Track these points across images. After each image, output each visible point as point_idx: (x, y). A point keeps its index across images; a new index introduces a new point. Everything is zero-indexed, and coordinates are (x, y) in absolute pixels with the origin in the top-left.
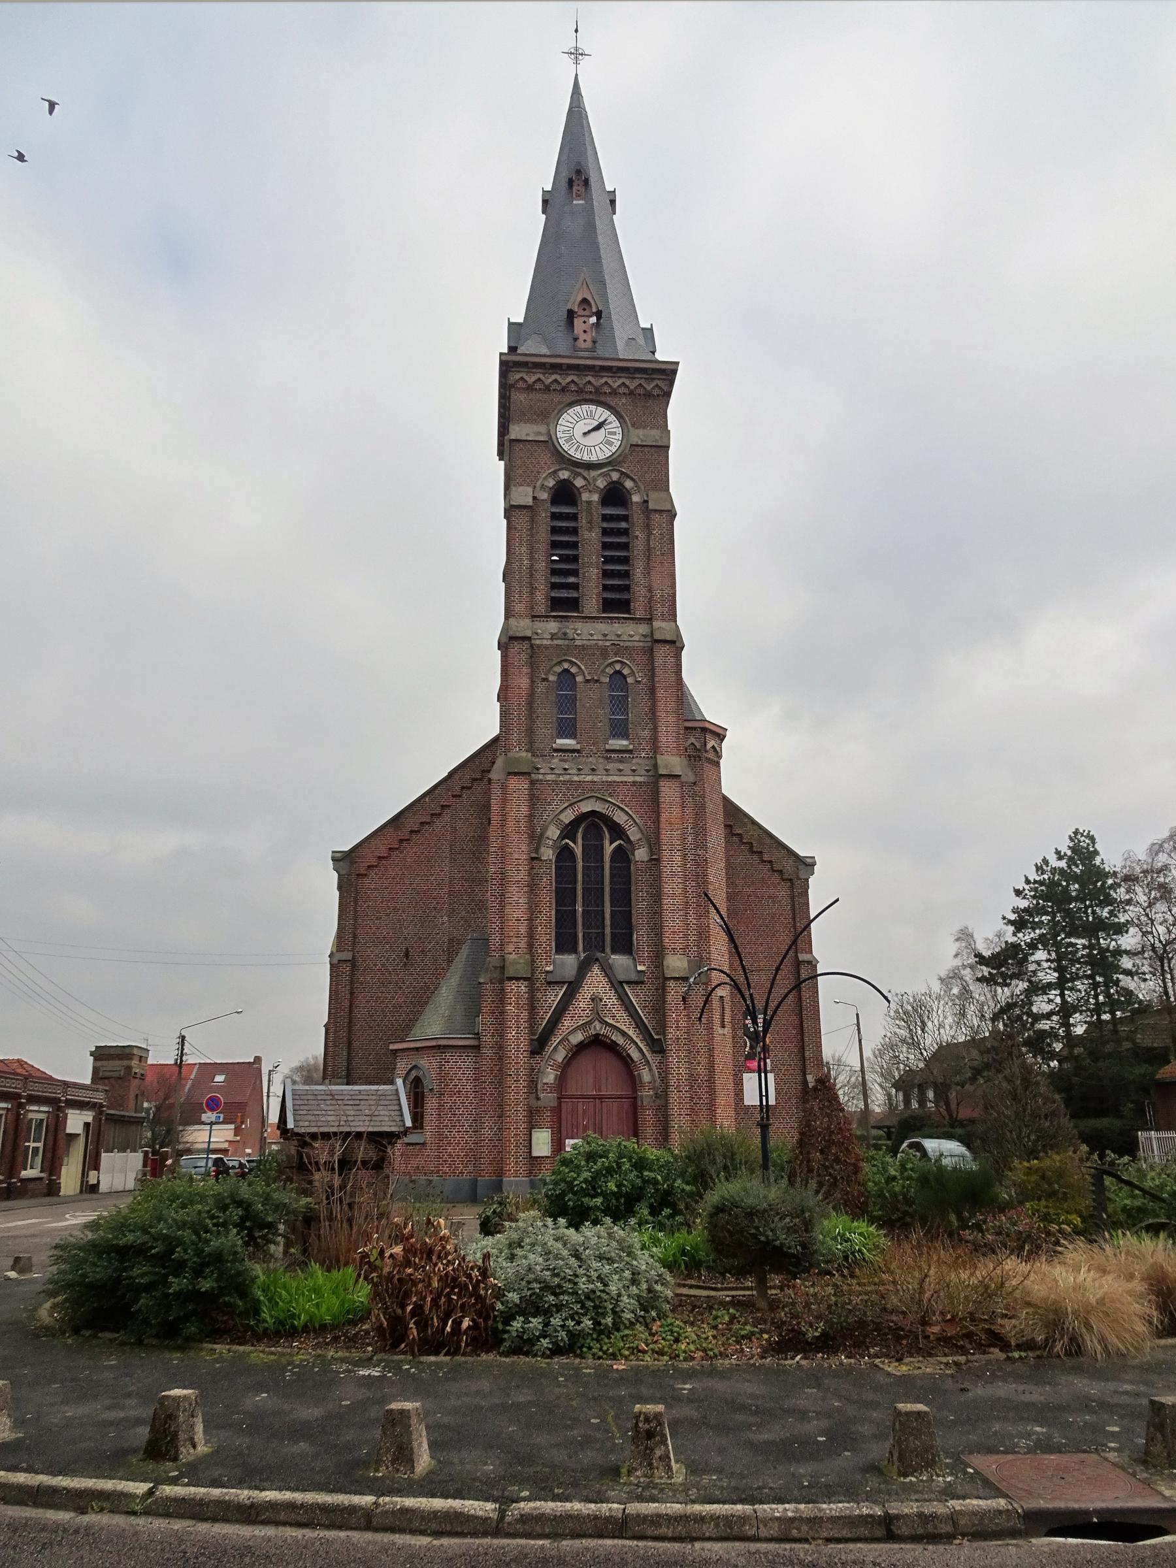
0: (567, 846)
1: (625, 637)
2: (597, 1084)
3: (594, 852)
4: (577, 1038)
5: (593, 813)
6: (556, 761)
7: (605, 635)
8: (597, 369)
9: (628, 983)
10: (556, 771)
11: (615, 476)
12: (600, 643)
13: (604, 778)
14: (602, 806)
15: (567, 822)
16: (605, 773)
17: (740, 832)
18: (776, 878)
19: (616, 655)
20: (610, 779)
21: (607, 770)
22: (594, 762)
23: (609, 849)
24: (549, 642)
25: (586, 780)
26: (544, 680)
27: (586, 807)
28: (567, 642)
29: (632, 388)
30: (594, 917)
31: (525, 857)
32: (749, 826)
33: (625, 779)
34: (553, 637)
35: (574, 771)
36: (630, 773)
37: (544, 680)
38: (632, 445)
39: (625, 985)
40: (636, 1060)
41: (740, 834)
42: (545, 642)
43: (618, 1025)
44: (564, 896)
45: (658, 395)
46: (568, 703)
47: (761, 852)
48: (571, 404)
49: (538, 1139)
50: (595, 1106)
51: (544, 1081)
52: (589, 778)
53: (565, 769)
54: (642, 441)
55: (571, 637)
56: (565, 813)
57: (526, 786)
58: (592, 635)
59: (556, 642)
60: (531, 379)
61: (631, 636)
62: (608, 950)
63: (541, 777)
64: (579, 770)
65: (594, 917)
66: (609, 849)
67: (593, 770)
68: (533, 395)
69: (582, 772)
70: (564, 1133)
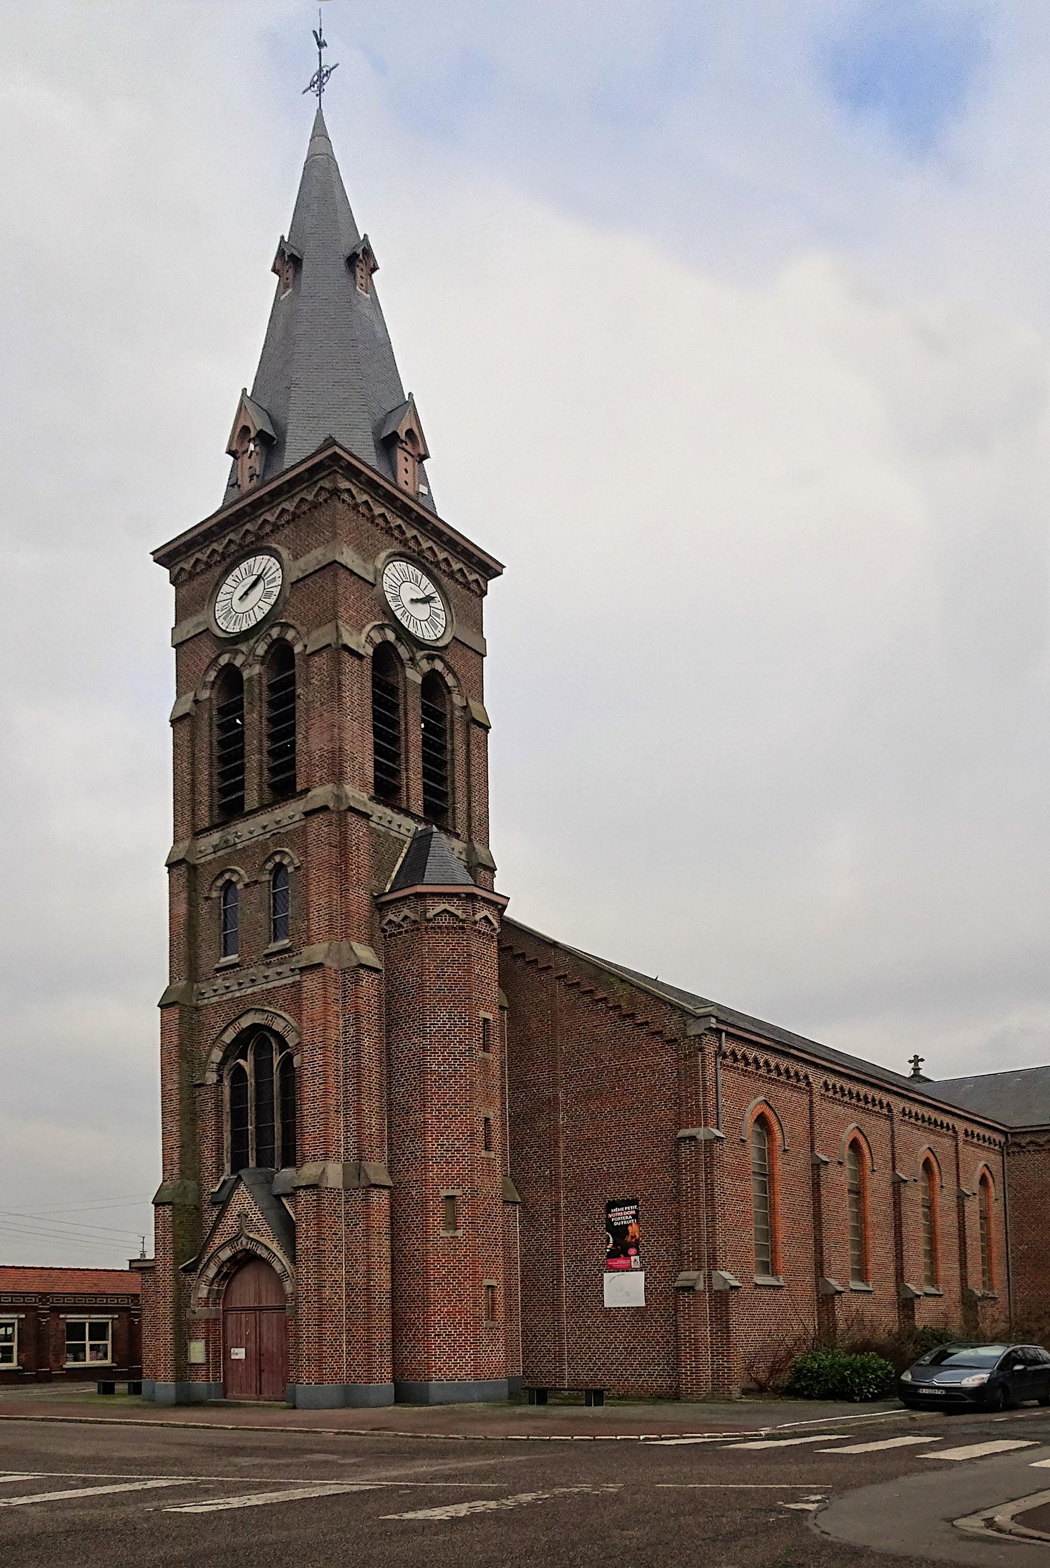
0: (239, 1065)
1: (285, 822)
2: (258, 1296)
3: (262, 1068)
4: (226, 1254)
5: (254, 1027)
6: (220, 981)
7: (264, 827)
8: (267, 499)
9: (286, 1195)
10: (220, 992)
11: (275, 632)
12: (261, 838)
13: (265, 987)
14: (262, 1017)
15: (228, 1042)
16: (264, 980)
17: (605, 995)
18: (657, 1043)
19: (276, 845)
20: (270, 986)
21: (266, 977)
22: (255, 972)
23: (277, 1059)
24: (213, 856)
25: (247, 993)
26: (207, 899)
27: (246, 1022)
28: (229, 850)
29: (292, 509)
30: (264, 1134)
31: (177, 1086)
32: (617, 985)
33: (285, 982)
34: (216, 849)
35: (236, 987)
36: (290, 973)
37: (207, 899)
38: (292, 584)
39: (284, 1201)
40: (279, 1272)
41: (605, 999)
42: (209, 858)
43: (261, 1239)
44: (238, 1118)
45: (325, 501)
46: (227, 920)
47: (633, 1015)
48: (227, 572)
49: (194, 1349)
50: (256, 1316)
51: (199, 1296)
52: (250, 991)
53: (228, 988)
54: (303, 571)
55: (232, 842)
56: (227, 1033)
57: (177, 1016)
58: (251, 833)
59: (219, 854)
60: (203, 556)
61: (291, 817)
62: (277, 1163)
63: (206, 1001)
64: (240, 984)
65: (264, 1134)
66: (277, 1059)
67: (253, 981)
68: (200, 579)
69: (242, 987)
70: (229, 1343)
